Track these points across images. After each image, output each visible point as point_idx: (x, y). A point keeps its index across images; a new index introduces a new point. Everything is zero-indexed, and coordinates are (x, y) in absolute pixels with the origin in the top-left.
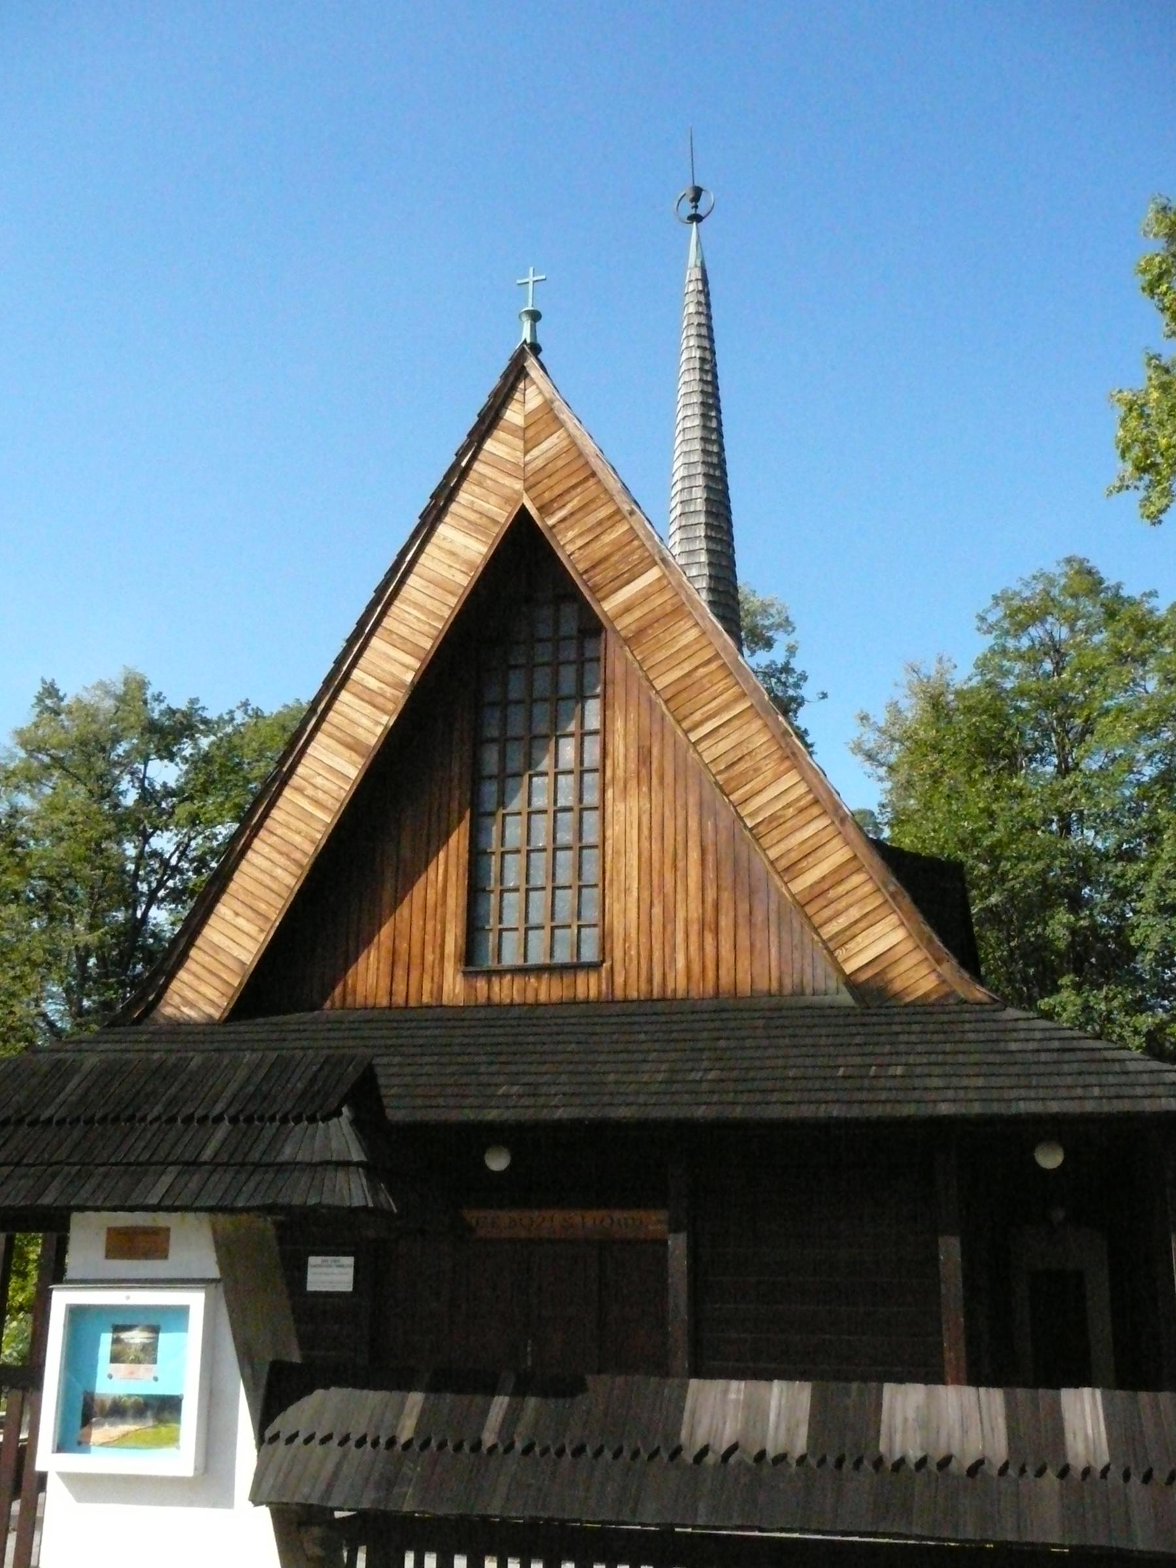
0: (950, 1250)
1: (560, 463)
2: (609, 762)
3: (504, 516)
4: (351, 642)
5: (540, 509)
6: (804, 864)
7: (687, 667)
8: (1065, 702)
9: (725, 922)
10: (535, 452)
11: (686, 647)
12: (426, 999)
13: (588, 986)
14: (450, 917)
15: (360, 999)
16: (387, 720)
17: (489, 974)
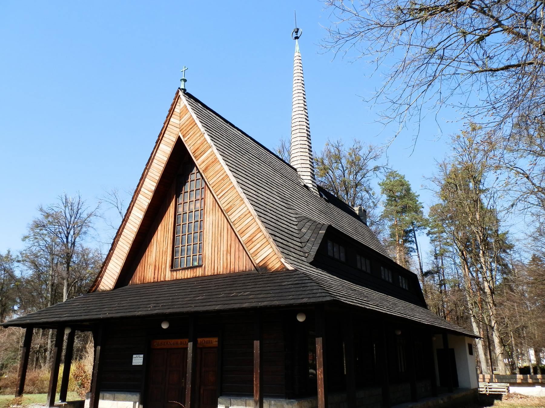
0: (257, 343)
1: (188, 122)
2: (206, 207)
3: (175, 140)
4: (141, 180)
5: (183, 136)
6: (246, 231)
7: (218, 176)
8: (52, 250)
9: (233, 250)
10: (182, 120)
11: (218, 171)
12: (162, 279)
13: (199, 272)
14: (168, 255)
15: (147, 281)
16: (149, 201)
17: (176, 270)
